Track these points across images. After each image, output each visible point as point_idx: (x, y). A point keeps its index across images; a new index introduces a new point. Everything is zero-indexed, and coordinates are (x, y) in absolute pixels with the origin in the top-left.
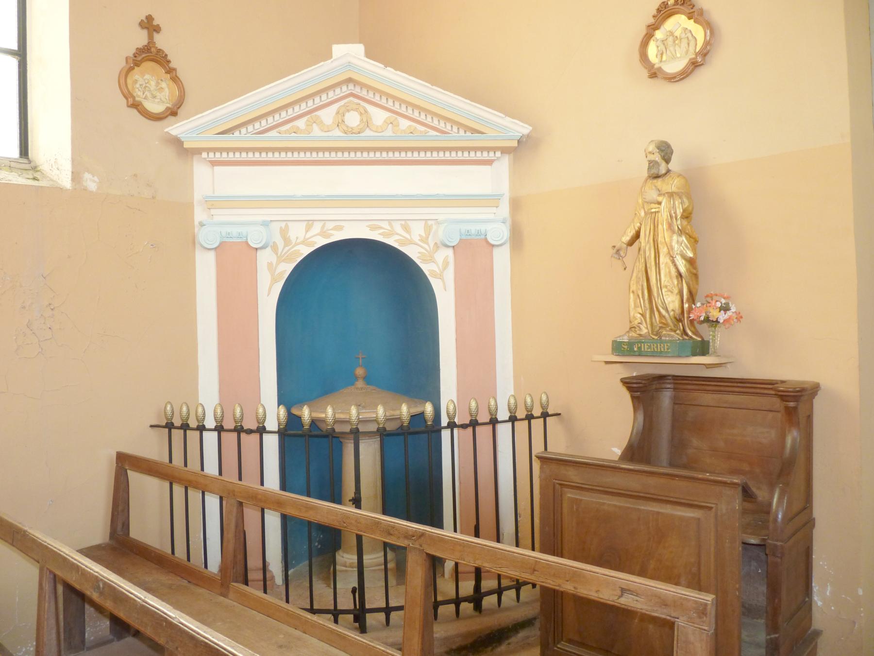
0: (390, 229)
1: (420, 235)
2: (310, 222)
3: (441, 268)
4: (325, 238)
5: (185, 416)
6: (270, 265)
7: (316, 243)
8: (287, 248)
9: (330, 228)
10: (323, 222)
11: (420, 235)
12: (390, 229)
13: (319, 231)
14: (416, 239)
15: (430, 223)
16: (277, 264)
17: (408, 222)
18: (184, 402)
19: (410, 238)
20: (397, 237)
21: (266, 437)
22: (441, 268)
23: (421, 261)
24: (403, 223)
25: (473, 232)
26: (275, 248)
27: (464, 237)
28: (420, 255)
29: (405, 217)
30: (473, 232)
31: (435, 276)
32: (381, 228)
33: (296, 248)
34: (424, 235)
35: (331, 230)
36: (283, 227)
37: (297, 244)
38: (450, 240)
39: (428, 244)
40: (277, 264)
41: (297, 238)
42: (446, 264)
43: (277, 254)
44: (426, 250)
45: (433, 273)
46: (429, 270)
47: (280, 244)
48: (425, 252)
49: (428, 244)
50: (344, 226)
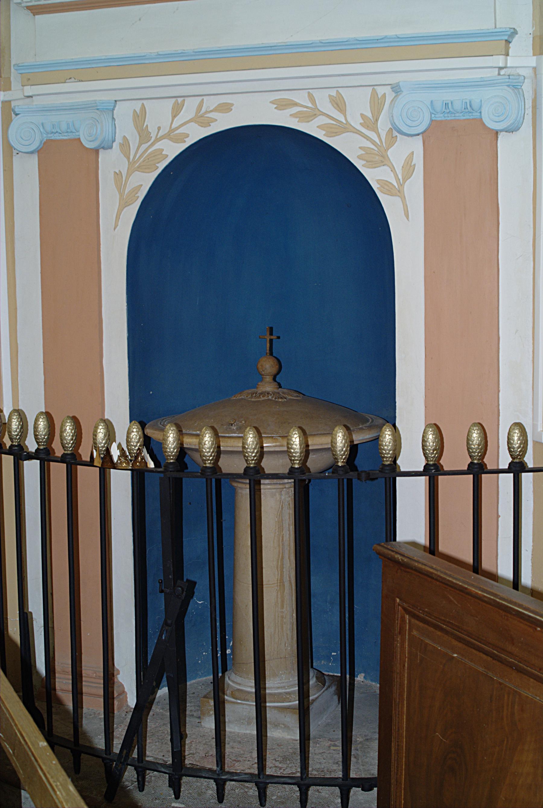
0: (310, 105)
1: (362, 115)
2: (180, 100)
3: (400, 177)
4: (202, 126)
5: (476, 449)
6: (118, 175)
7: (187, 136)
8: (144, 146)
9: (211, 108)
10: (200, 99)
11: (362, 115)
12: (310, 105)
13: (192, 115)
14: (356, 123)
15: (380, 91)
16: (129, 175)
17: (375, 87)
18: (474, 424)
19: (344, 122)
20: (322, 120)
21: (266, 486)
22: (400, 177)
23: (364, 162)
24: (333, 93)
25: (458, 106)
26: (125, 146)
27: (440, 117)
28: (363, 152)
29: (308, 83)
30: (458, 106)
31: (390, 191)
32: (296, 104)
33: (157, 146)
34: (369, 115)
35: (211, 111)
36: (138, 111)
37: (157, 140)
38: (409, 122)
39: (375, 129)
40: (129, 175)
41: (159, 128)
42: (409, 169)
43: (128, 158)
44: (373, 142)
45: (385, 184)
46: (378, 181)
47: (134, 140)
48: (372, 146)
49: (375, 129)
50: (232, 105)
